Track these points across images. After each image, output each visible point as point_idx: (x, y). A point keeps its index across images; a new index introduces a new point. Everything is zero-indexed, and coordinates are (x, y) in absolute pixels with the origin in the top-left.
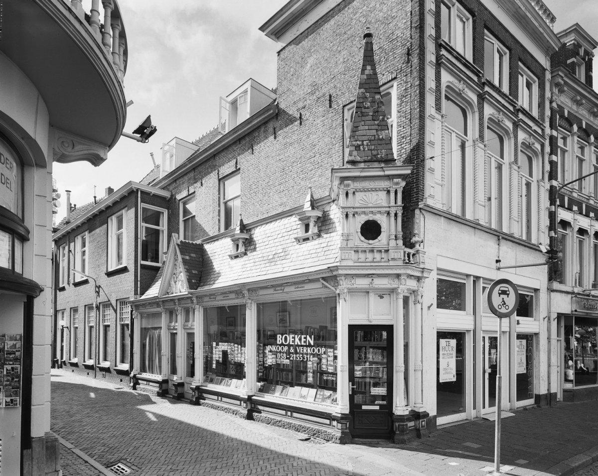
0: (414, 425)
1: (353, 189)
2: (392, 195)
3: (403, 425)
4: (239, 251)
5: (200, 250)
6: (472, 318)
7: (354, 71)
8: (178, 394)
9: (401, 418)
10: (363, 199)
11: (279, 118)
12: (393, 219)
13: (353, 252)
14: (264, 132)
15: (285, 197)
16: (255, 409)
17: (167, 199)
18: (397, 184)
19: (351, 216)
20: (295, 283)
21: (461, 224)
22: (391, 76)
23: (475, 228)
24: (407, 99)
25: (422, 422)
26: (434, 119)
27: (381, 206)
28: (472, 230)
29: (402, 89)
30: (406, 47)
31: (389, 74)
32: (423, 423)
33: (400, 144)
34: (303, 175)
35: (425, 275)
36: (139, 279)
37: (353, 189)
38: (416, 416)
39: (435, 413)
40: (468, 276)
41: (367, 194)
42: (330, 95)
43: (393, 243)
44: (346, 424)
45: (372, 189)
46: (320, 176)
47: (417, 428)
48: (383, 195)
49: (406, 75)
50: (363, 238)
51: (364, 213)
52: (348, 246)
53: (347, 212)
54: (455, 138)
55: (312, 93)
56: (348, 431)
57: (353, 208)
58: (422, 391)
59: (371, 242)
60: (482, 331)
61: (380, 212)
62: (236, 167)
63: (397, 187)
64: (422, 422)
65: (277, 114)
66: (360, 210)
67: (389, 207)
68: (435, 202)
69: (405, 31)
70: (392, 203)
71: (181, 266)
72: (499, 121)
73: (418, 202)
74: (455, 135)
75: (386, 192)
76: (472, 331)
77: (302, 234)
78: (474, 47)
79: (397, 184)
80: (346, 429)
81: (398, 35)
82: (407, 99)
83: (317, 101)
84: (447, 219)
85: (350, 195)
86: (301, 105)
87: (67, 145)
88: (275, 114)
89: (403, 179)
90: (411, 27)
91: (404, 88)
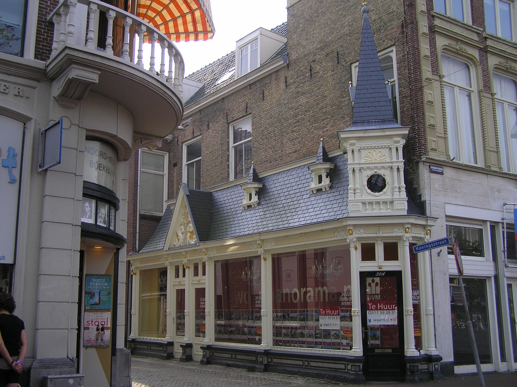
0: (427, 367)
1: (358, 147)
2: (394, 151)
3: (414, 366)
4: (252, 201)
5: (209, 197)
6: (492, 264)
7: (358, 35)
8: (186, 356)
9: (413, 360)
10: (367, 156)
11: (290, 68)
12: (395, 173)
13: (360, 204)
14: (276, 80)
15: (298, 145)
16: (272, 364)
17: (169, 141)
18: (398, 142)
19: (357, 171)
20: (101, 309)
21: (470, 172)
22: (390, 43)
23: (487, 174)
24: (405, 65)
25: (435, 365)
26: (431, 81)
27: (386, 162)
28: (486, 176)
29: (401, 55)
30: (401, 20)
31: (389, 41)
32: (436, 366)
33: (402, 103)
34: (316, 125)
35: (429, 224)
36: (138, 231)
37: (358, 147)
38: (429, 359)
39: (452, 359)
40: (485, 221)
41: (372, 151)
42: (338, 52)
43: (396, 195)
44: (360, 366)
45: (375, 147)
46: (332, 126)
47: (431, 371)
48: (386, 152)
49: (403, 44)
50: (369, 191)
51: (369, 168)
52: (356, 199)
53: (354, 168)
54: (458, 90)
55: (322, 49)
56: (361, 373)
57: (359, 164)
58: (435, 335)
59: (377, 194)
60: (505, 279)
61: (383, 167)
62: (246, 111)
63: (398, 145)
64: (435, 365)
65: (288, 65)
66: (365, 166)
67: (392, 163)
68: (438, 154)
69: (399, 7)
70: (395, 160)
71: (189, 216)
72: (507, 68)
73: (421, 155)
74: (457, 88)
75: (389, 149)
76: (493, 279)
77: (315, 185)
78: (472, 7)
79: (398, 142)
80: (359, 371)
81: (394, 9)
82: (405, 65)
83: (326, 56)
84: (454, 169)
85: (356, 153)
86: (311, 59)
87: (138, 142)
88: (286, 64)
89: (403, 138)
90: (404, 5)
91: (402, 55)
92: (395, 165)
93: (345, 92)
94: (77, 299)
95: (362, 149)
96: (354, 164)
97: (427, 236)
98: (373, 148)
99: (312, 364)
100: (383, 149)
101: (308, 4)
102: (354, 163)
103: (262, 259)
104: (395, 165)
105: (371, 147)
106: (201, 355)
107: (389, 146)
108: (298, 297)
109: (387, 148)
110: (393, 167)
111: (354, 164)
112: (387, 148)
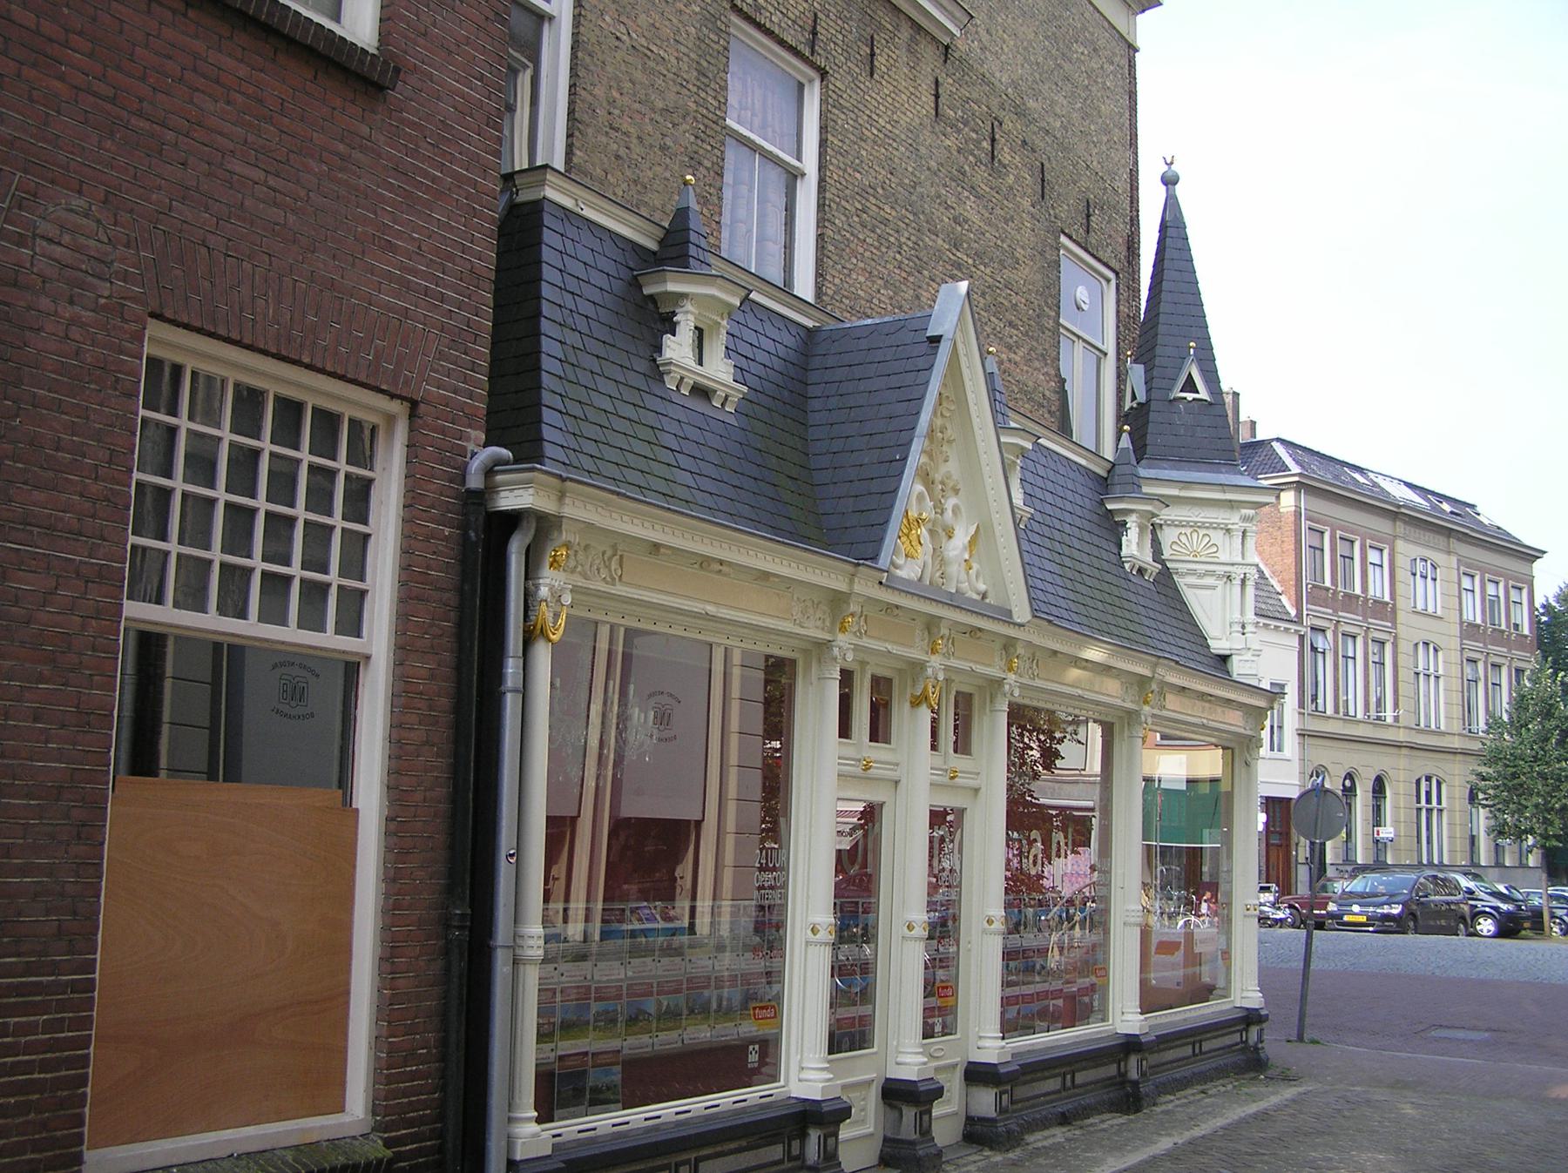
45: (1196, 522)
92: (1238, 572)
93: (81, 807)
94: (209, 673)
95: (1169, 525)
96: (1243, 564)
97: (840, 636)
98: (1191, 526)
99: (1206, 1046)
100: (1211, 530)
101: (291, 218)
102: (1243, 562)
103: (509, 696)
104: (1238, 572)
105: (1188, 522)
106: (513, 166)
107: (1226, 525)
108: (315, 519)
109: (1222, 529)
110: (1233, 575)
111: (1243, 564)
112: (1222, 529)
